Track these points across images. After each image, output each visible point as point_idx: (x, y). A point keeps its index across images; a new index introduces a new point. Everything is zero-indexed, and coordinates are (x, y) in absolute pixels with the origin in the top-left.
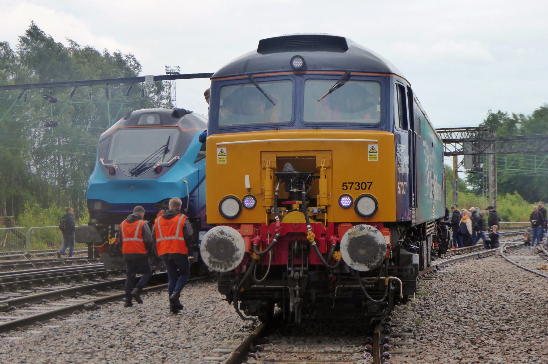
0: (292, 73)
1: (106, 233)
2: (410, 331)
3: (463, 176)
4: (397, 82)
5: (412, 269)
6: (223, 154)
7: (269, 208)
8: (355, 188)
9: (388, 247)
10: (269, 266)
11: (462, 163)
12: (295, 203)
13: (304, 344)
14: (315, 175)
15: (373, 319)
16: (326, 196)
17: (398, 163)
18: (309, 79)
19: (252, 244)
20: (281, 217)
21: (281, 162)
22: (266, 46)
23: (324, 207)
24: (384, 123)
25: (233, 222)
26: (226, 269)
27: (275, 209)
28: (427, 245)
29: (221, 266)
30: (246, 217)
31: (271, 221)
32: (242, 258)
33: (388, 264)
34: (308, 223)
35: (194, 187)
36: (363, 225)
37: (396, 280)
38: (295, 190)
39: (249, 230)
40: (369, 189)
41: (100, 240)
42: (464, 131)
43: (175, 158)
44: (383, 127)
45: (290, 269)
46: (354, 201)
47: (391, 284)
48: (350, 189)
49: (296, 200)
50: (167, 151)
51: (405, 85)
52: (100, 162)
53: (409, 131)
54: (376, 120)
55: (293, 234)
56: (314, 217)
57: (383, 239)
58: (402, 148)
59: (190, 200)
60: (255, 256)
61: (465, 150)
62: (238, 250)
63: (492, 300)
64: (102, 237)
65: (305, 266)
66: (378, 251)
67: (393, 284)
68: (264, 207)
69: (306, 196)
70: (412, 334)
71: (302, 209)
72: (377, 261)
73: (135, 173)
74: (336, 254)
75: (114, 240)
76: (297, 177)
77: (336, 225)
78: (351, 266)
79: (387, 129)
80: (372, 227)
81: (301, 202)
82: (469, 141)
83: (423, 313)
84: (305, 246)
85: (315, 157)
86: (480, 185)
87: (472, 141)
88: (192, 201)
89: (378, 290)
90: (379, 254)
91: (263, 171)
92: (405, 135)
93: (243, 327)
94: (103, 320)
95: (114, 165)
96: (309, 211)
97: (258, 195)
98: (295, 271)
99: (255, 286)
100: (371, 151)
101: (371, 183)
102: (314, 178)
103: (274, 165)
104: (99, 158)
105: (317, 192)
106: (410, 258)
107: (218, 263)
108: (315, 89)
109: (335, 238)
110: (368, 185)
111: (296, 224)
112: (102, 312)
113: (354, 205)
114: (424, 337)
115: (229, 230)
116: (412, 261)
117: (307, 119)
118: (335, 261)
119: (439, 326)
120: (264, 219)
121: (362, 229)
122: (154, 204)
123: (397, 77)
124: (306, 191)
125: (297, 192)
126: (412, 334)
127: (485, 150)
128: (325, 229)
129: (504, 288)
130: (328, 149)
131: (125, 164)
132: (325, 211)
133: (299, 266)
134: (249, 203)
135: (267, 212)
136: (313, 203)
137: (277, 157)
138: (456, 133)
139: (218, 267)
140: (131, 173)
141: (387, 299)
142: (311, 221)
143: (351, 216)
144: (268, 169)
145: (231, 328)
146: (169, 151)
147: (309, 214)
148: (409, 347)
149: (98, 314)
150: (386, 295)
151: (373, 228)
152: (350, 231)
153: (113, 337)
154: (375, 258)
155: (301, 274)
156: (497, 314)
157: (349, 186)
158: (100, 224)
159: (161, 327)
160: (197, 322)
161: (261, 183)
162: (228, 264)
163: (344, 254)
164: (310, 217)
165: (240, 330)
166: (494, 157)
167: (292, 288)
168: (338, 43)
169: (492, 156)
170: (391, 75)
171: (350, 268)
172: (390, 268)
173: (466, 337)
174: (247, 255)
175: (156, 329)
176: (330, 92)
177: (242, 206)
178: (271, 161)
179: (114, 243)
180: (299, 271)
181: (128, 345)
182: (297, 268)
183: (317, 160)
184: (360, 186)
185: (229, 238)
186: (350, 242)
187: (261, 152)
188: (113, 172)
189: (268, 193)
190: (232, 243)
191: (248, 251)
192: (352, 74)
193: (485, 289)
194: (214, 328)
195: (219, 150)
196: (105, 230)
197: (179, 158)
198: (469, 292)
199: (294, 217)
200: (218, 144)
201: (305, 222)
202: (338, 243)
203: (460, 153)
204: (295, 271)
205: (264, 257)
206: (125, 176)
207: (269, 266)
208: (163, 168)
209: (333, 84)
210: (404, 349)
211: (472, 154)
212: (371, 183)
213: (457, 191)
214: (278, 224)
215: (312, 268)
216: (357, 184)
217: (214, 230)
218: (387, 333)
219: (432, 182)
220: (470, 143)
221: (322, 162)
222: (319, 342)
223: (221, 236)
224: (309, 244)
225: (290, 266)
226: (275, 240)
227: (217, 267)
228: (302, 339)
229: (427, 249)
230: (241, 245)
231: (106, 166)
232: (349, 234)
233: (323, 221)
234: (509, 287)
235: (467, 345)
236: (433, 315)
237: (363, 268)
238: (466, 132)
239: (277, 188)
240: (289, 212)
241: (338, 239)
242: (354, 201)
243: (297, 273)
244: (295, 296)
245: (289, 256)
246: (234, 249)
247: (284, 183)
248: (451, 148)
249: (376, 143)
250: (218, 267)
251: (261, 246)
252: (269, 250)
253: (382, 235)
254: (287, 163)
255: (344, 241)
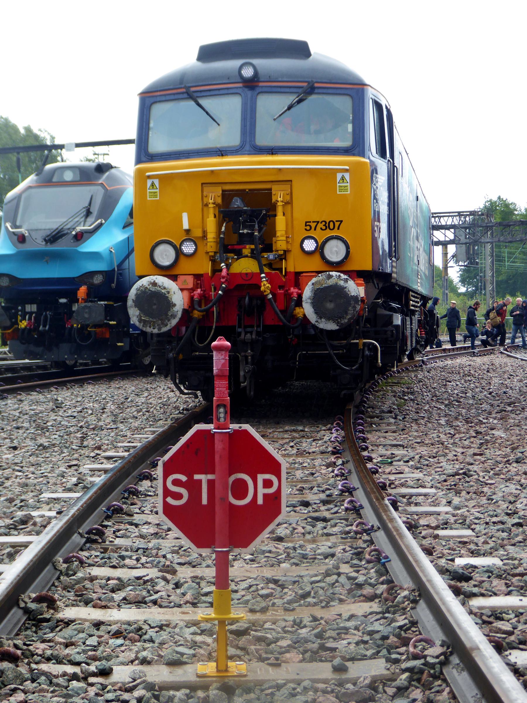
0: (240, 85)
1: (15, 316)
2: (390, 412)
3: (454, 273)
4: (373, 97)
5: (392, 331)
6: (155, 187)
7: (212, 254)
8: (321, 229)
9: (363, 300)
10: (214, 327)
11: (453, 257)
12: (245, 248)
13: (259, 425)
14: (270, 213)
15: (343, 392)
16: (284, 238)
17: (375, 198)
18: (262, 92)
19: (192, 299)
20: (228, 266)
21: (227, 196)
22: (208, 53)
23: (282, 252)
24: (357, 147)
25: (169, 272)
26: (159, 329)
27: (220, 256)
28: (411, 324)
29: (154, 326)
30: (187, 267)
31: (216, 270)
32: (179, 315)
33: (362, 325)
34: (262, 272)
35: (123, 257)
36: (331, 273)
37: (373, 343)
38: (245, 231)
39: (190, 282)
40: (338, 229)
41: (8, 323)
42: (456, 216)
43: (99, 221)
44: (356, 152)
45: (240, 330)
46: (320, 244)
47: (366, 349)
48: (315, 229)
49: (248, 244)
50: (88, 213)
51: (383, 103)
52: (6, 228)
53: (389, 161)
54: (347, 143)
55: (247, 285)
56: (270, 265)
57: (356, 289)
58: (379, 180)
59: (118, 274)
60: (196, 314)
61: (457, 239)
62: (175, 305)
63: (492, 387)
64: (10, 319)
65: (258, 326)
66: (350, 304)
67: (369, 349)
68: (207, 253)
69: (260, 238)
70: (393, 415)
71: (254, 255)
72: (348, 317)
73: (50, 240)
74: (298, 310)
75: (25, 324)
76: (247, 213)
77: (298, 274)
78: (316, 324)
79: (362, 154)
80: (342, 275)
81: (253, 247)
82: (462, 228)
83: (406, 398)
84: (259, 302)
85: (270, 189)
86: (475, 287)
87: (466, 228)
88: (121, 274)
89: (351, 354)
90: (350, 308)
91: (205, 209)
92: (382, 165)
93: (183, 410)
94: (10, 409)
95: (22, 230)
96: (263, 257)
97: (199, 237)
98: (246, 333)
99: (197, 353)
100: (341, 181)
101: (341, 221)
102: (269, 216)
103: (219, 201)
104: (5, 224)
105: (273, 232)
106: (390, 319)
107: (149, 322)
108: (270, 105)
109: (296, 290)
110: (337, 224)
111: (247, 274)
112: (9, 401)
113: (320, 249)
114: (407, 416)
115: (162, 281)
116: (392, 322)
117: (261, 140)
118: (297, 319)
119: (426, 408)
120: (206, 268)
121: (330, 277)
122: (74, 278)
123: (373, 90)
124: (259, 233)
125: (248, 233)
126: (393, 415)
127: (481, 238)
128: (284, 280)
129: (506, 376)
130: (285, 179)
131: (37, 230)
132: (283, 257)
133: (252, 327)
134: (188, 248)
135: (210, 260)
136: (269, 248)
137: (223, 191)
138: (446, 218)
139: (150, 327)
140: (45, 240)
141: (361, 367)
142: (266, 270)
143: (315, 264)
144: (211, 206)
145: (168, 411)
146: (91, 213)
147: (264, 262)
148: (389, 424)
149: (4, 403)
150: (360, 360)
151: (343, 276)
152: (314, 280)
153: (21, 420)
154: (347, 314)
155: (254, 337)
156: (497, 398)
157: (313, 225)
158: (8, 305)
159: (81, 412)
160: (126, 406)
161: (203, 222)
162: (162, 323)
163: (308, 310)
164: (265, 265)
165: (180, 412)
166: (492, 248)
167: (243, 354)
168: (300, 49)
169: (489, 246)
170: (365, 87)
171: (314, 327)
172: (365, 329)
173: (460, 417)
174: (185, 312)
175: (75, 414)
176: (289, 108)
177: (179, 252)
178: (214, 196)
179: (26, 327)
180: (251, 333)
181: (38, 427)
182: (249, 329)
183: (273, 192)
184: (327, 226)
185: (163, 291)
186: (314, 294)
187: (202, 184)
188: (22, 239)
189: (211, 235)
190: (168, 297)
191: (186, 308)
192: (316, 85)
193: (482, 378)
194: (148, 412)
195: (149, 182)
196: (13, 311)
197: (103, 221)
198: (463, 381)
199: (245, 266)
200: (148, 174)
201: (259, 271)
202: (300, 296)
203: (451, 242)
204: (246, 333)
205: (208, 313)
206: (37, 244)
207: (214, 327)
208: (84, 235)
209: (292, 98)
210: (384, 427)
211: (466, 244)
212: (341, 221)
213: (446, 291)
214: (224, 273)
215: (267, 328)
216: (324, 223)
217: (144, 282)
218: (362, 413)
219: (417, 244)
220: (463, 230)
221: (279, 196)
222: (278, 423)
223: (153, 289)
224: (263, 297)
225: (240, 327)
226: (220, 292)
227: (148, 328)
228: (256, 420)
229: (411, 329)
230: (179, 300)
231: (14, 233)
232: (313, 284)
233: (281, 270)
234: (511, 375)
235: (460, 424)
236: (419, 400)
237: (331, 326)
238: (458, 218)
239: (223, 229)
240: (237, 259)
241: (300, 291)
242: (320, 244)
243: (248, 336)
244: (247, 363)
245: (238, 315)
246: (170, 305)
247: (232, 223)
248: (439, 235)
249: (347, 171)
250: (150, 327)
251: (203, 301)
252: (214, 304)
253: (355, 285)
254: (235, 198)
255: (307, 292)
